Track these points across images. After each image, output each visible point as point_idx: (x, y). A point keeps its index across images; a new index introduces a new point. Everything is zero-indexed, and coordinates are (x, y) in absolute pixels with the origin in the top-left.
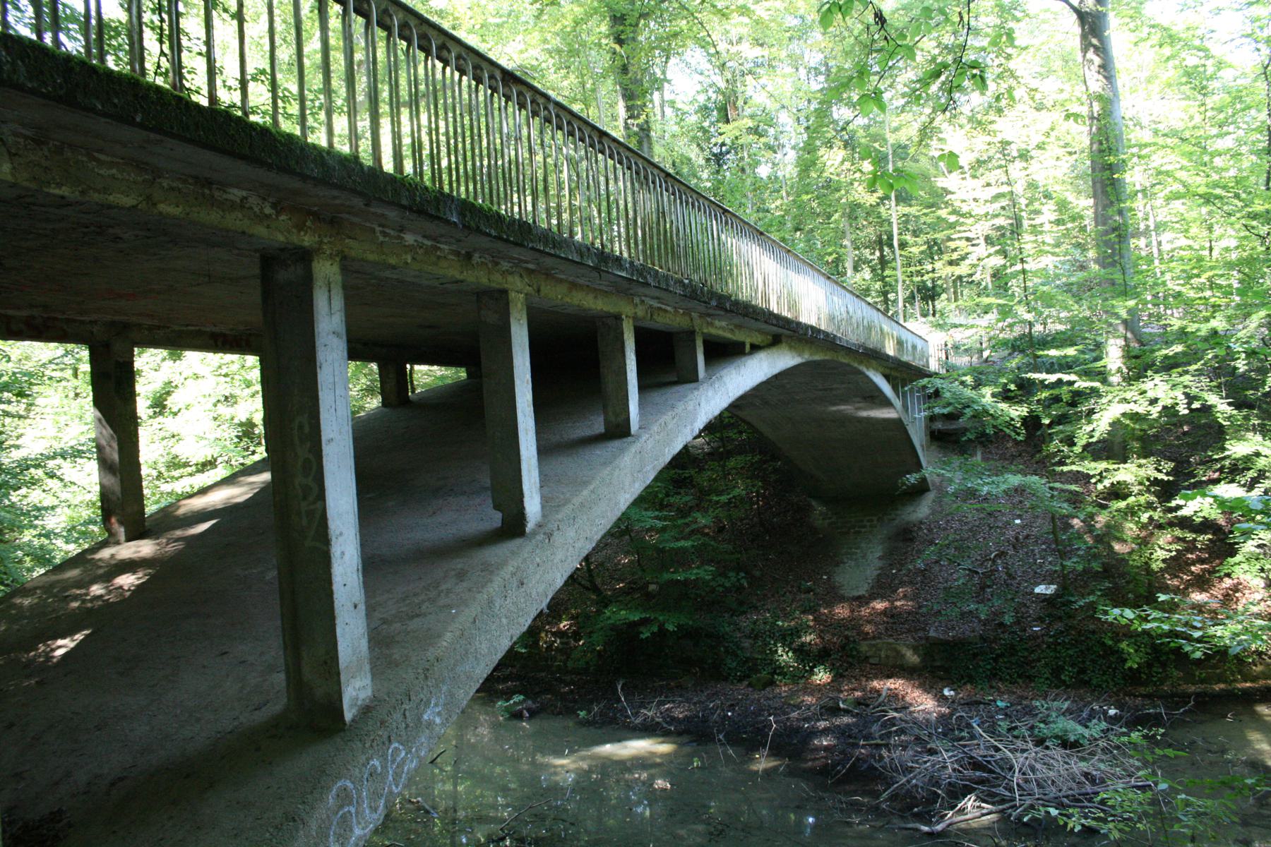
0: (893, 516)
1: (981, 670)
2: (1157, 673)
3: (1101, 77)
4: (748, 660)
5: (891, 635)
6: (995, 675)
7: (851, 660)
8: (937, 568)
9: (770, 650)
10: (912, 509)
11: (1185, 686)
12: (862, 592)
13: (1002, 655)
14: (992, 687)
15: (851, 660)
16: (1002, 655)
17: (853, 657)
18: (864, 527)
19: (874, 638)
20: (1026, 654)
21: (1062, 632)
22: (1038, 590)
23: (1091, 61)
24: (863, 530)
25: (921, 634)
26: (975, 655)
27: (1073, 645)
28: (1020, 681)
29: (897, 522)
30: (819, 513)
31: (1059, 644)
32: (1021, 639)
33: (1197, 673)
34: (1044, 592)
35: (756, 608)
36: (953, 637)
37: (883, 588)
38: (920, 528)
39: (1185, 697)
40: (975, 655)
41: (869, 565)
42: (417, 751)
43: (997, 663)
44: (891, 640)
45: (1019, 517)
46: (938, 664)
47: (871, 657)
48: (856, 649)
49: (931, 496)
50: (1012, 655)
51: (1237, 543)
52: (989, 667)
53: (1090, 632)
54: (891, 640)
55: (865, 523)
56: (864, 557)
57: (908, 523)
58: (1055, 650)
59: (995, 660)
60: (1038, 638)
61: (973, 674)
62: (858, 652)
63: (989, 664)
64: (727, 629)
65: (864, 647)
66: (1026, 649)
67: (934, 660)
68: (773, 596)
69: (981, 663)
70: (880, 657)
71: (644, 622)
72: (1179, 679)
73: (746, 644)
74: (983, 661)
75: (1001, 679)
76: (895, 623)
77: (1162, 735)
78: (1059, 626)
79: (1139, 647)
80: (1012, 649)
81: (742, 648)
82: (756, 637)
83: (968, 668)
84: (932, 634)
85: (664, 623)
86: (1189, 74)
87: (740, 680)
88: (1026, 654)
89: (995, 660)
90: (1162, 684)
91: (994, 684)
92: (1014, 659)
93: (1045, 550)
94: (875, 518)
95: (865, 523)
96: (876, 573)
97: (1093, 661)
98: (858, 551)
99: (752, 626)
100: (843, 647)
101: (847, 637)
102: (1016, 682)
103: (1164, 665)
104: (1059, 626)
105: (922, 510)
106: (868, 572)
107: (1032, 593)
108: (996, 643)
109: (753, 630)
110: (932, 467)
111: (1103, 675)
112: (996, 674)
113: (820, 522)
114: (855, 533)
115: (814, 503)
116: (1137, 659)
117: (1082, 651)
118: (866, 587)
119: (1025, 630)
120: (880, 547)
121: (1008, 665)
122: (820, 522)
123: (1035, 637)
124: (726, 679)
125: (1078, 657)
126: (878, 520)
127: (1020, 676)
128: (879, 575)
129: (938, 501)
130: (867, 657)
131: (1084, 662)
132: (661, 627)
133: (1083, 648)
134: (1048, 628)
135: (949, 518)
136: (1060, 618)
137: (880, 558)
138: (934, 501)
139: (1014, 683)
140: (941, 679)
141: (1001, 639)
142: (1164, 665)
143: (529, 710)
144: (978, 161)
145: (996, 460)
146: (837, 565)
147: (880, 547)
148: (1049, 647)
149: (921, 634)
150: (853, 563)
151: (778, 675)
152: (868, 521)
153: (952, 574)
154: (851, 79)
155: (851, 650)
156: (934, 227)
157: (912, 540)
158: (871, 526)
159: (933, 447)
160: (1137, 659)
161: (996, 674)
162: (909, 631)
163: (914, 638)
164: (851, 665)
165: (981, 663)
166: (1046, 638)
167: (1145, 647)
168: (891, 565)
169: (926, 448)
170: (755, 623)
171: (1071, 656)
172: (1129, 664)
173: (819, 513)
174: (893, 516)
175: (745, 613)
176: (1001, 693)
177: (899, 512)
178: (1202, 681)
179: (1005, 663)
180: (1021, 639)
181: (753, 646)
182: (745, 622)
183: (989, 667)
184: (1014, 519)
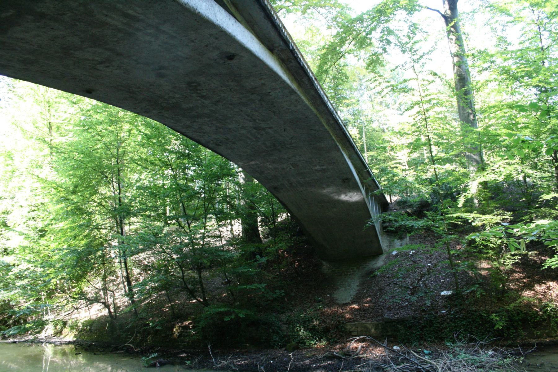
0: (364, 266)
1: (414, 335)
2: (513, 333)
3: (456, 45)
4: (285, 336)
5: (364, 319)
6: (422, 338)
7: (341, 333)
8: (388, 288)
9: (297, 330)
10: (374, 262)
11: (529, 340)
12: (347, 301)
13: (425, 327)
14: (420, 345)
15: (341, 333)
16: (425, 327)
17: (343, 332)
18: (350, 272)
19: (354, 321)
20: (439, 325)
21: (458, 312)
22: (442, 293)
23: (452, 39)
24: (349, 273)
25: (380, 318)
26: (410, 327)
27: (464, 319)
28: (436, 341)
29: (366, 269)
30: (326, 267)
31: (457, 319)
32: (436, 317)
33: (535, 333)
34: (446, 294)
35: (291, 310)
36: (398, 317)
37: (357, 299)
39: (531, 345)
40: (410, 327)
41: (352, 289)
43: (422, 331)
44: (363, 322)
45: (430, 262)
46: (390, 334)
47: (352, 332)
48: (344, 327)
49: (383, 257)
50: (431, 326)
51: (554, 247)
52: (418, 333)
53: (473, 311)
54: (363, 322)
56: (349, 286)
57: (372, 269)
58: (455, 322)
59: (422, 329)
60: (445, 316)
61: (409, 337)
62: (345, 329)
63: (418, 331)
64: (274, 319)
65: (348, 327)
66: (438, 323)
67: (388, 332)
68: (300, 304)
69: (414, 332)
70: (357, 331)
71: (227, 313)
72: (526, 336)
73: (284, 327)
74: (414, 330)
75: (425, 340)
76: (365, 314)
77: (523, 361)
78: (456, 309)
79: (502, 318)
80: (431, 323)
81: (282, 330)
82: (289, 324)
83: (407, 335)
84: (386, 316)
85: (238, 314)
87: (281, 348)
88: (439, 325)
89: (422, 329)
90: (516, 339)
91: (422, 343)
92: (431, 329)
93: (445, 276)
94: (355, 268)
96: (356, 292)
97: (476, 327)
99: (288, 318)
100: (337, 327)
101: (339, 321)
102: (434, 342)
103: (516, 328)
104: (456, 309)
105: (380, 262)
106: (352, 293)
107: (439, 295)
108: (421, 320)
109: (288, 319)
110: (384, 242)
111: (482, 335)
112: (423, 337)
116: (501, 324)
117: (470, 322)
118: (350, 299)
119: (437, 313)
120: (358, 281)
121: (429, 332)
123: (443, 316)
124: (273, 348)
125: (468, 325)
127: (436, 338)
128: (357, 293)
129: (388, 258)
130: (350, 332)
131: (471, 328)
132: (237, 316)
133: (470, 320)
134: (450, 310)
136: (456, 306)
137: (357, 286)
138: (385, 258)
139: (433, 342)
140: (392, 342)
141: (424, 317)
142: (516, 328)
143: (160, 363)
145: (416, 239)
146: (335, 290)
148: (451, 321)
149: (380, 318)
151: (301, 343)
152: (352, 269)
153: (396, 290)
155: (341, 328)
156: (384, 161)
159: (384, 235)
160: (501, 324)
161: (423, 337)
162: (373, 317)
163: (376, 320)
164: (342, 336)
165: (414, 332)
166: (449, 316)
167: (505, 318)
168: (363, 288)
169: (382, 236)
170: (289, 316)
171: (464, 325)
172: (497, 326)
173: (326, 267)
174: (364, 266)
175: (284, 312)
176: (426, 348)
177: (368, 264)
178: (538, 337)
179: (427, 331)
180: (436, 317)
181: (287, 328)
182: (284, 317)
183: (418, 333)
184: (427, 264)
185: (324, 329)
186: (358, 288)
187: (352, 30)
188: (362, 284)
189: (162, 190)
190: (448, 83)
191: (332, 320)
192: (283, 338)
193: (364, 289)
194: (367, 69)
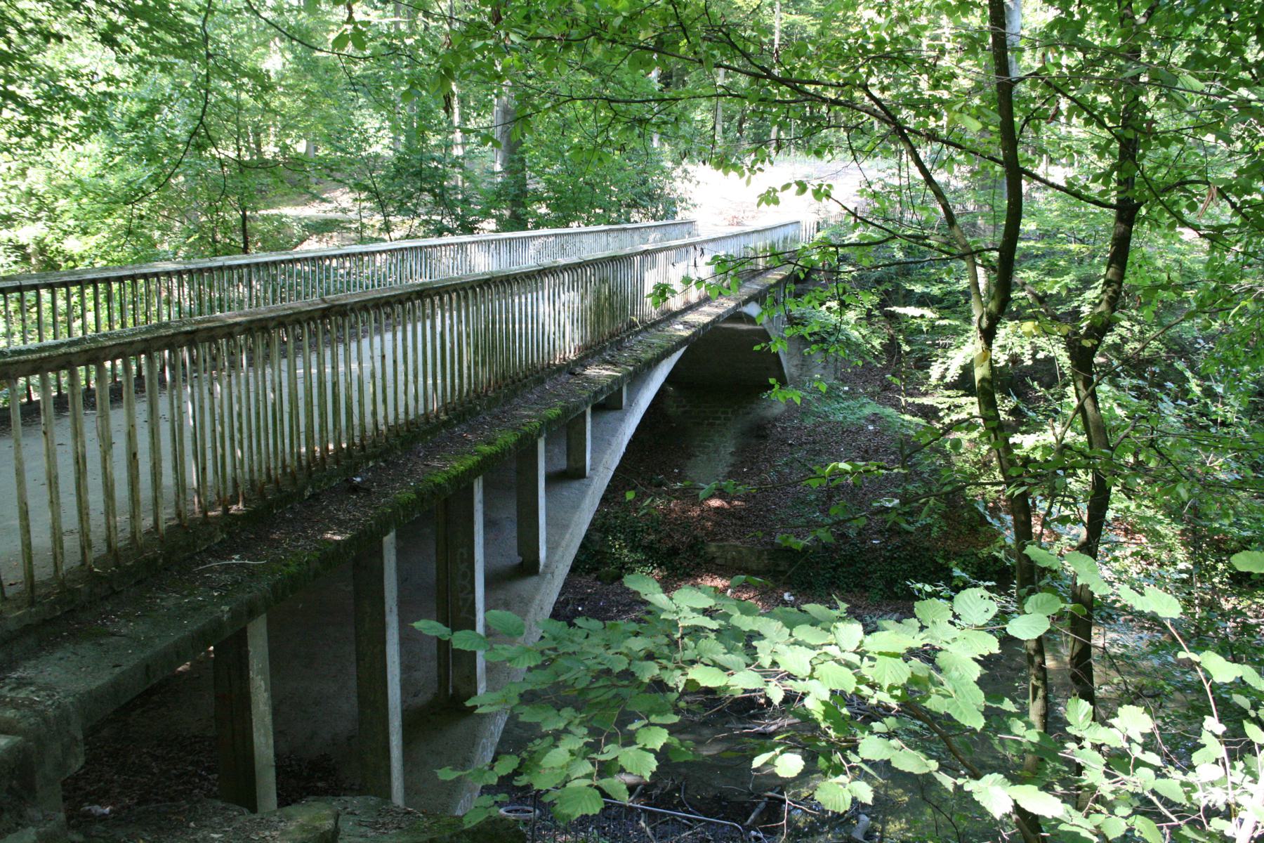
6: (833, 583)
13: (841, 565)
16: (841, 565)
18: (719, 418)
28: (856, 590)
50: (851, 565)
57: (763, 419)
58: (890, 564)
59: (835, 569)
80: (851, 560)
87: (588, 573)
89: (835, 569)
94: (730, 411)
100: (691, 547)
117: (915, 567)
123: (873, 549)
127: (856, 586)
185: (668, 550)
186: (732, 460)
187: (833, 339)
188: (740, 451)
189: (331, 465)
190: (1048, 601)
191: (682, 535)
192: (594, 556)
193: (743, 464)
194: (830, 186)
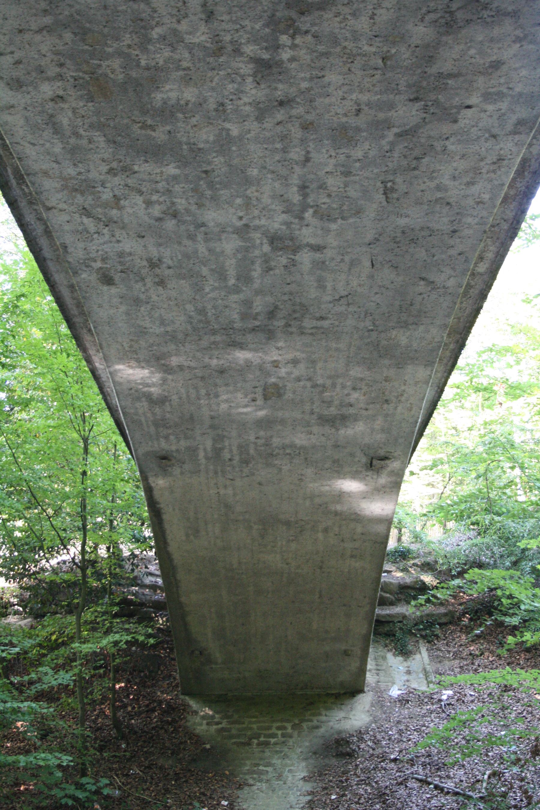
10: (341, 714)
18: (274, 736)
24: (273, 740)
29: (322, 730)
38: (361, 739)
42: (423, 793)
55: (274, 730)
56: (279, 777)
57: (339, 732)
86: (156, 11)
94: (289, 726)
95: (274, 730)
98: (269, 769)
106: (292, 798)
113: (204, 727)
114: (259, 744)
115: (193, 704)
122: (204, 727)
126: (293, 727)
135: (402, 727)
138: (372, 705)
144: (66, 247)
147: (304, 764)
150: (264, 786)
152: (278, 728)
154: (509, 13)
157: (351, 755)
158: (283, 736)
174: (315, 723)
177: (324, 718)
